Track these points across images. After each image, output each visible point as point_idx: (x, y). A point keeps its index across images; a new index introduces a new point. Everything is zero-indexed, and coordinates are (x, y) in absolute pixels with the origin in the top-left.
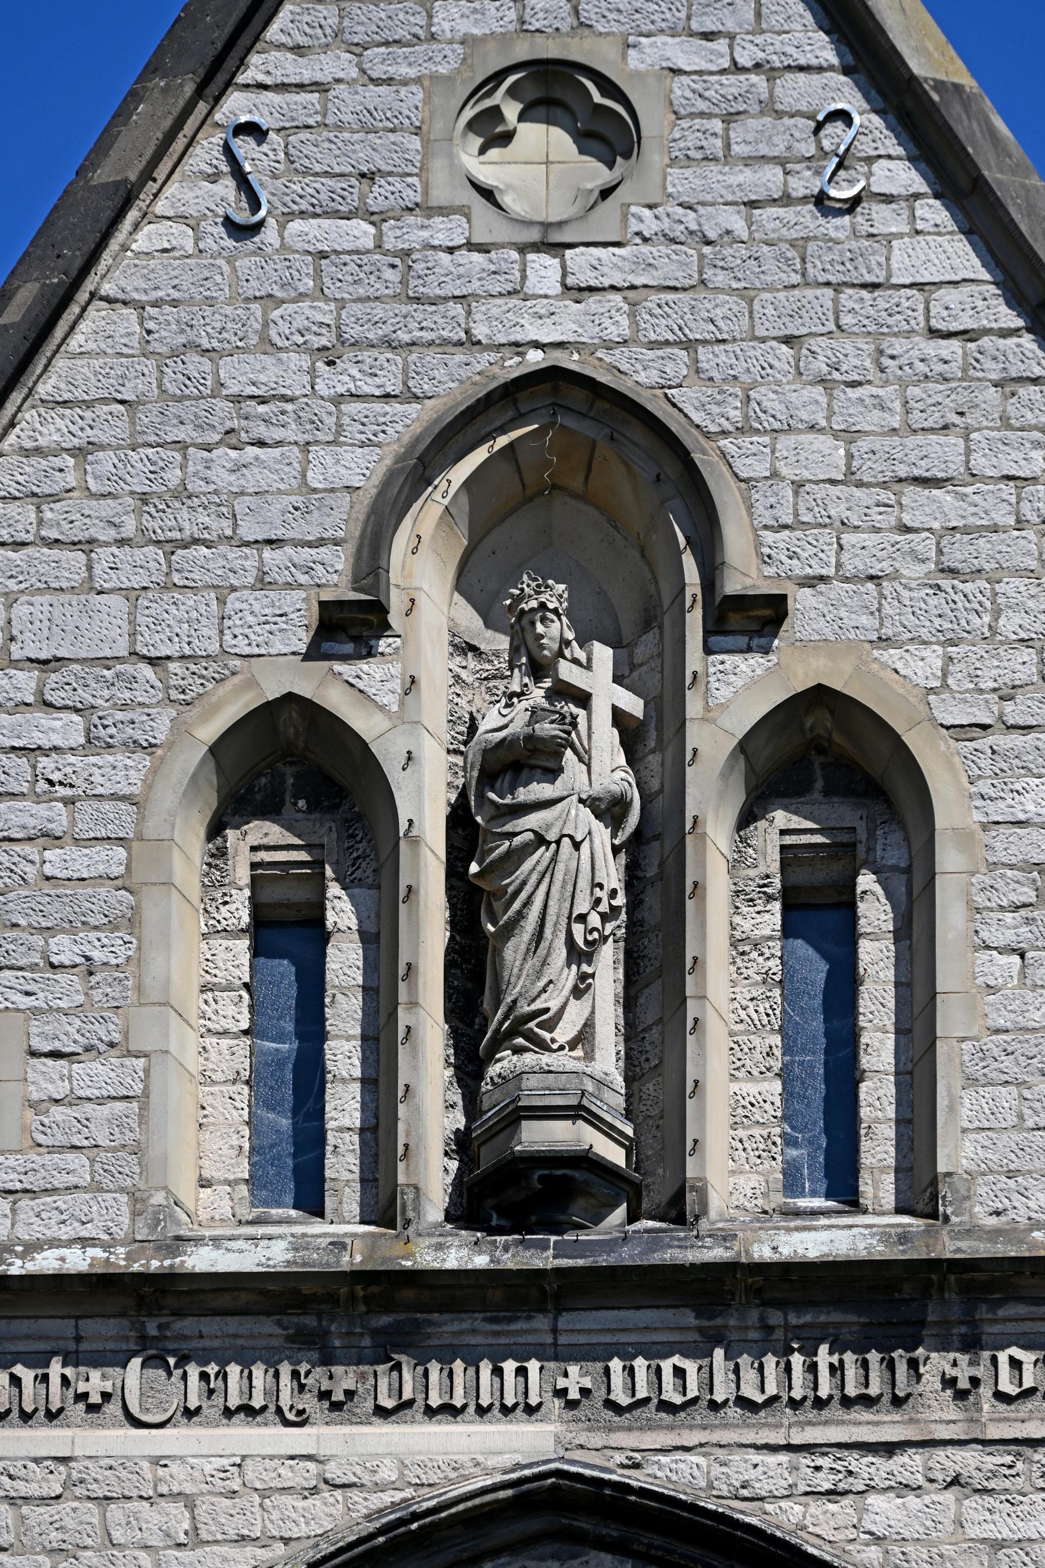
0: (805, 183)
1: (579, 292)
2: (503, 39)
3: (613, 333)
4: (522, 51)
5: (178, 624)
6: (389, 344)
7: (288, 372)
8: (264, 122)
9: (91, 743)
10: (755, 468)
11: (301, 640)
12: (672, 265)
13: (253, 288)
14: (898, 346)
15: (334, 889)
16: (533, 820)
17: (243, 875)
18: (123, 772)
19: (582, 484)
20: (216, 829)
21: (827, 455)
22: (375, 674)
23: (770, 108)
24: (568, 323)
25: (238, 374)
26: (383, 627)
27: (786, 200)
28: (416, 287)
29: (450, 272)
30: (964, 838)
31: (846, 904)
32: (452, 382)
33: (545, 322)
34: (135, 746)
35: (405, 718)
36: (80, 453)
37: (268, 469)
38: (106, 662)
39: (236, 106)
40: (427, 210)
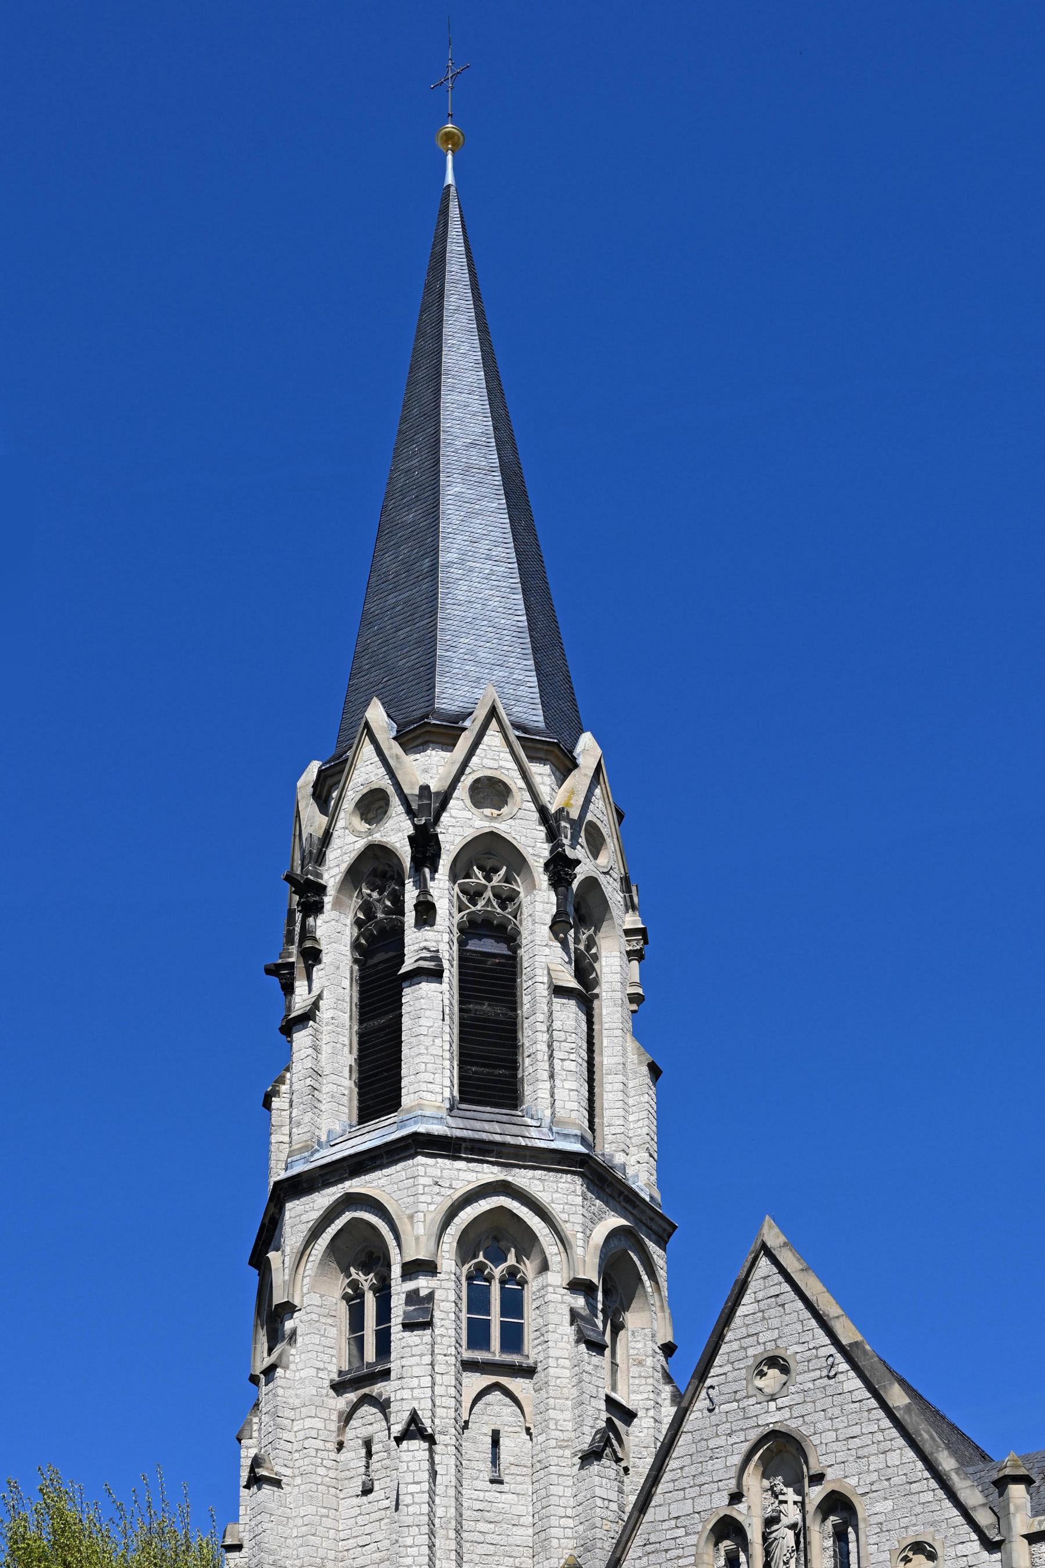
0: (825, 1373)
1: (779, 1409)
2: (761, 1354)
3: (787, 1417)
4: (765, 1356)
5: (702, 1504)
6: (742, 1430)
7: (721, 1441)
8: (714, 1384)
9: (687, 1534)
10: (817, 1442)
11: (727, 1502)
12: (798, 1398)
13: (714, 1423)
14: (845, 1407)
15: (741, 1553)
16: (774, 1535)
17: (723, 1553)
18: (693, 1539)
19: (781, 1453)
20: (716, 1544)
21: (832, 1435)
22: (742, 1507)
23: (817, 1357)
24: (778, 1417)
25: (712, 1444)
26: (743, 1496)
27: (821, 1378)
28: (747, 1416)
29: (753, 1410)
30: (865, 1520)
31: (846, 1534)
32: (754, 1435)
33: (772, 1417)
34: (695, 1533)
35: (749, 1516)
36: (681, 1468)
37: (719, 1464)
38: (688, 1515)
39: (709, 1382)
40: (748, 1397)
